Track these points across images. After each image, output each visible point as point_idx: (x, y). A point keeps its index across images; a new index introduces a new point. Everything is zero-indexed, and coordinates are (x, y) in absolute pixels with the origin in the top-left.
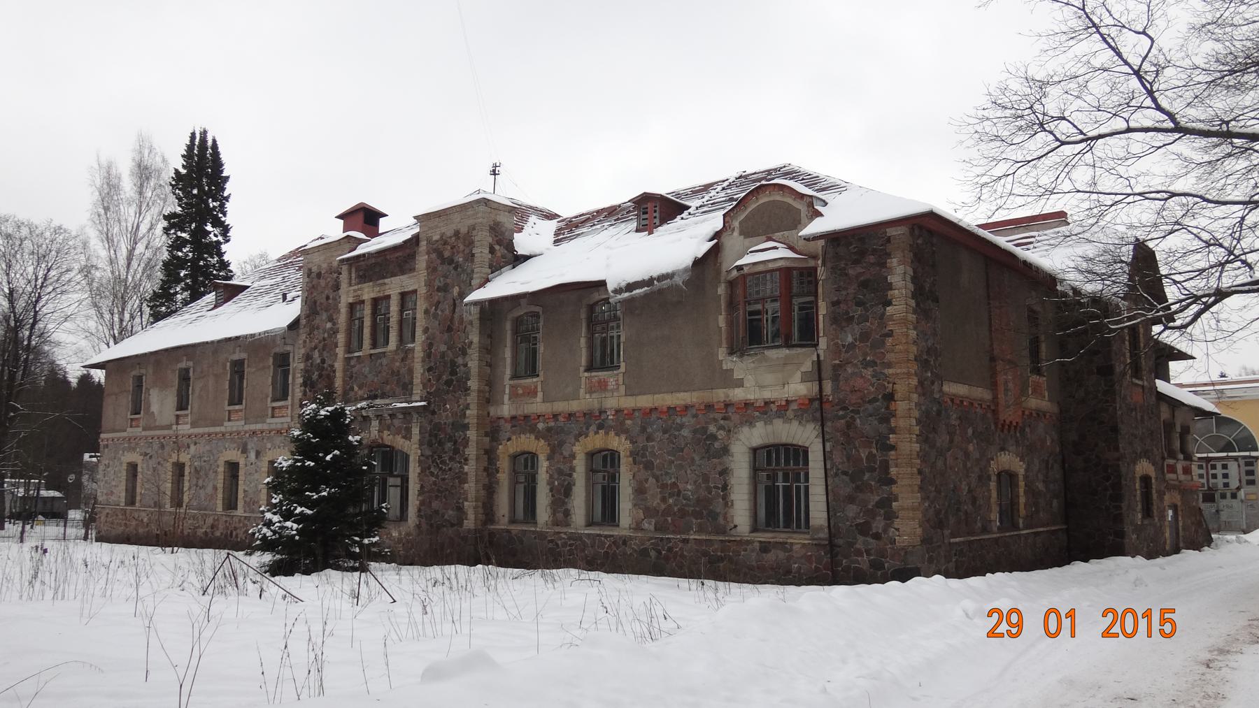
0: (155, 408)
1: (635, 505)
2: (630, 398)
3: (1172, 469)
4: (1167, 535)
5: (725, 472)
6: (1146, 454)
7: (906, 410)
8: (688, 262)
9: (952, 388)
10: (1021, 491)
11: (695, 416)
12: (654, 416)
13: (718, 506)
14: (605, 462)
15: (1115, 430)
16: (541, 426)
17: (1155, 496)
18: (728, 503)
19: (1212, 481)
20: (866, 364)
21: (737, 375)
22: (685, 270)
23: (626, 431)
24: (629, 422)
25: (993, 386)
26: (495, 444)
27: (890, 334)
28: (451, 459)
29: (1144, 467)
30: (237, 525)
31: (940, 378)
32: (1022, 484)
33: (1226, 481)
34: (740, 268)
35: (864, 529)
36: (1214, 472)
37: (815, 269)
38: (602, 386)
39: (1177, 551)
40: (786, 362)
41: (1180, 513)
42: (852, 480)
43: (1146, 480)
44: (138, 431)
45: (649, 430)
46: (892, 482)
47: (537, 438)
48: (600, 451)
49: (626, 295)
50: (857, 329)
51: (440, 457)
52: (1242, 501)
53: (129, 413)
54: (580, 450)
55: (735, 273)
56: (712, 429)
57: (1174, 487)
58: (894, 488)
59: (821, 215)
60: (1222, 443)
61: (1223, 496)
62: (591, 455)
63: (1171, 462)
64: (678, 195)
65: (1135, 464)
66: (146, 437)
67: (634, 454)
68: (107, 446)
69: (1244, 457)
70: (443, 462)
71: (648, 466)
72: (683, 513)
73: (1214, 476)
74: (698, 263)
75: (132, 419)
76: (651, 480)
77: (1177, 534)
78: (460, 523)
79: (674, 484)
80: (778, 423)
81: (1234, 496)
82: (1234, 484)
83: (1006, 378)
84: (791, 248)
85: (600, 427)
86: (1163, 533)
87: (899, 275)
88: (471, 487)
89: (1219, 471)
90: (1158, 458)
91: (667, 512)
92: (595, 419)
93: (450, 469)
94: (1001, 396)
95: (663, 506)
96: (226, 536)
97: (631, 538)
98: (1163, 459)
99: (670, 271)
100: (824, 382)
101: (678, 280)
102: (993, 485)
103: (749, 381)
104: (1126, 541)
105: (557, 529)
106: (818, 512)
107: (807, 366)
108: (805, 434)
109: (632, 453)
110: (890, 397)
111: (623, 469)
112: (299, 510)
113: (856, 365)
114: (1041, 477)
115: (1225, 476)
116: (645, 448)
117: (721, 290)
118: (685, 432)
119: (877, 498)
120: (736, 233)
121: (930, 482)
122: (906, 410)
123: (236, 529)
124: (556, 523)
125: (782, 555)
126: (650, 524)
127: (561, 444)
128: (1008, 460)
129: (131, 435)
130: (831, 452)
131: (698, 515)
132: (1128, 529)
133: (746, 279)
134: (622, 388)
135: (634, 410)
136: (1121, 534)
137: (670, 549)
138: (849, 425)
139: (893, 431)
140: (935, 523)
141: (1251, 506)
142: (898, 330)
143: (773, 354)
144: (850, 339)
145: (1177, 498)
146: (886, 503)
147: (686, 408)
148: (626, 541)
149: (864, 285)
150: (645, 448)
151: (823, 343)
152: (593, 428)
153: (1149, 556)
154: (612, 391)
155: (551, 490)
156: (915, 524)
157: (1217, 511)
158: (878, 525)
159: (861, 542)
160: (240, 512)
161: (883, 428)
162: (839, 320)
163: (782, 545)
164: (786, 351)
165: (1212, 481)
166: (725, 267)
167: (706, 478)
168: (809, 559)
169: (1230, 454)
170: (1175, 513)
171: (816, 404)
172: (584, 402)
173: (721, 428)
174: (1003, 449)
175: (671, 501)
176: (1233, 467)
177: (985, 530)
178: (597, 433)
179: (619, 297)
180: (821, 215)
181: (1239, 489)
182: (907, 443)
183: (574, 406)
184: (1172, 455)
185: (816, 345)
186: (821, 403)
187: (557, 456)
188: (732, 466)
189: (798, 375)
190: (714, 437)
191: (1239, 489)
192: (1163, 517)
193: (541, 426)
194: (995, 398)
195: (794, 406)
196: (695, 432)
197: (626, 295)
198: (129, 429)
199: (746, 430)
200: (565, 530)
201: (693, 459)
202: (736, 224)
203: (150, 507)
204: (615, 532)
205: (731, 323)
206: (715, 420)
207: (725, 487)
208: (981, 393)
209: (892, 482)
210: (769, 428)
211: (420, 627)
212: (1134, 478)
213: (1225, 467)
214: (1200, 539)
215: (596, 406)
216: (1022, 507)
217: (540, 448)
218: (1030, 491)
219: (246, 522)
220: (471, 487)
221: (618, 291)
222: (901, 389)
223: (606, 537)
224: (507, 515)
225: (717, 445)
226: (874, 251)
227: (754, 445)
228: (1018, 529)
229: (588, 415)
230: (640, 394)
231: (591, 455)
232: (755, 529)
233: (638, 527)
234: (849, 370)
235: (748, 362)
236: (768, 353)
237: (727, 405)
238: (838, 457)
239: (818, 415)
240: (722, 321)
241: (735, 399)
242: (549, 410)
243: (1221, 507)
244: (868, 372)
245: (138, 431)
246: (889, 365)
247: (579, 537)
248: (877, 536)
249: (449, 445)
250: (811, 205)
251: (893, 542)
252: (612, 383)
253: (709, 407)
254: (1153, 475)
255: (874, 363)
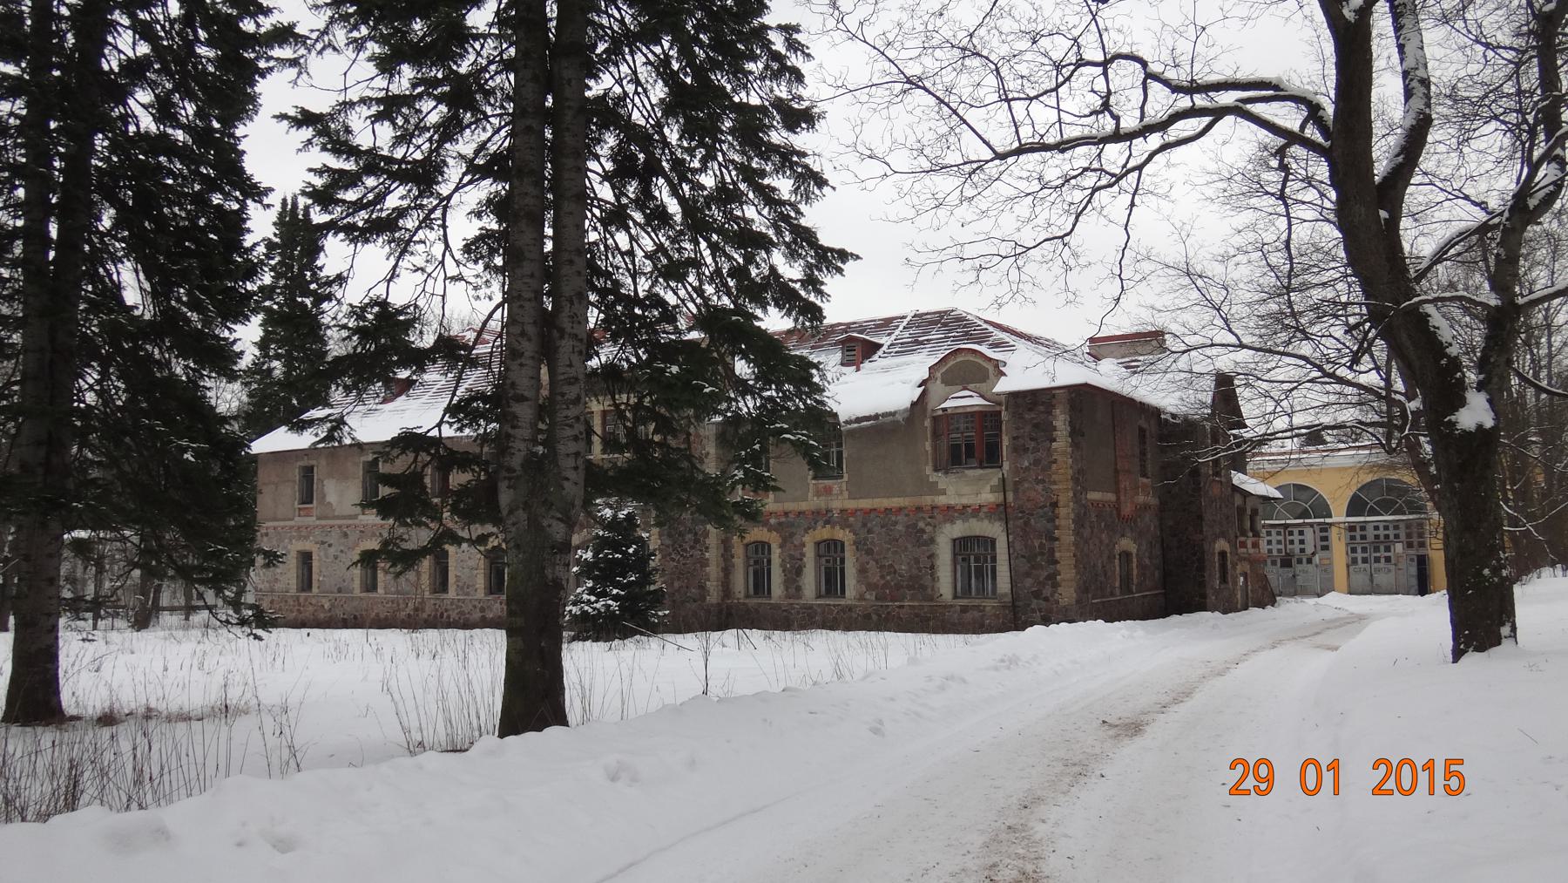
0: (332, 497)
1: (858, 582)
2: (852, 501)
3: (1243, 545)
4: (1239, 596)
5: (932, 556)
6: (1223, 535)
7: (1066, 513)
8: (908, 405)
9: (1094, 496)
10: (1134, 565)
11: (907, 515)
12: (872, 515)
13: (927, 581)
14: (831, 549)
15: (1200, 517)
16: (772, 521)
17: (1229, 566)
18: (934, 579)
19: (1289, 547)
20: (1038, 482)
21: (941, 486)
22: (905, 410)
23: (849, 526)
24: (851, 519)
25: (1117, 492)
26: (729, 535)
27: (1055, 461)
28: (692, 548)
29: (1222, 545)
30: (449, 607)
31: (1085, 490)
32: (1135, 560)
33: (1302, 546)
34: (944, 410)
35: (1037, 595)
36: (1291, 538)
37: (1000, 412)
38: (828, 491)
39: (1246, 608)
40: (980, 479)
41: (1249, 580)
42: (1029, 562)
43: (1223, 554)
44: (311, 520)
45: (869, 525)
46: (1057, 562)
47: (769, 531)
48: (825, 541)
49: (856, 425)
50: (1032, 457)
51: (681, 546)
52: (1317, 566)
53: (296, 503)
54: (809, 540)
55: (940, 413)
56: (921, 525)
57: (1245, 559)
58: (1058, 566)
59: (1004, 374)
60: (1299, 511)
61: (1299, 561)
62: (818, 544)
63: (1243, 539)
64: (861, 327)
65: (1215, 543)
66: (323, 527)
67: (857, 544)
68: (267, 535)
69: (1319, 524)
70: (685, 550)
71: (869, 552)
72: (898, 587)
73: (1279, 542)
74: (913, 404)
75: (300, 509)
76: (872, 563)
77: (1247, 595)
78: (703, 598)
79: (891, 566)
80: (973, 521)
81: (1309, 561)
82: (1309, 550)
83: (1125, 483)
84: (982, 396)
85: (827, 522)
86: (1236, 595)
87: (1061, 421)
88: (713, 570)
89: (1296, 538)
90: (1232, 536)
91: (886, 585)
92: (823, 516)
93: (692, 556)
94: (1122, 498)
95: (882, 582)
96: (435, 616)
97: (857, 606)
98: (1236, 537)
99: (893, 410)
100: (1007, 493)
101: (899, 418)
102: (1117, 562)
103: (951, 490)
104: (1208, 601)
105: (791, 601)
106: (1004, 583)
107: (995, 481)
108: (995, 530)
109: (855, 543)
110: (1055, 505)
111: (847, 554)
112: (615, 591)
113: (1030, 482)
114: (1147, 554)
115: (1302, 542)
116: (866, 539)
117: (928, 423)
118: (899, 527)
119: (1046, 574)
120: (939, 382)
121: (1081, 562)
122: (1066, 513)
123: (446, 610)
124: (788, 597)
125: (976, 614)
126: (871, 595)
127: (792, 535)
128: (1127, 544)
129: (300, 524)
130: (1013, 542)
131: (910, 587)
132: (1209, 592)
133: (950, 417)
134: (846, 494)
135: (856, 510)
136: (1204, 596)
137: (889, 613)
138: (1027, 523)
139: (1057, 528)
140: (1083, 589)
141: (1325, 571)
142: (1059, 458)
143: (970, 473)
144: (1026, 464)
145: (1247, 567)
146: (1052, 576)
147: (900, 509)
148: (850, 608)
149: (1036, 426)
150: (866, 539)
151: (1006, 466)
152: (820, 523)
153: (1225, 612)
154: (837, 495)
155: (784, 571)
156: (1072, 590)
157: (1294, 576)
158: (1047, 591)
159: (1035, 603)
160: (452, 593)
161: (1049, 526)
162: (1019, 450)
163: (977, 607)
164: (980, 471)
165: (1289, 547)
166: (930, 407)
167: (917, 561)
168: (997, 616)
169: (1307, 521)
170: (1246, 579)
171: (1002, 508)
172: (812, 502)
173: (929, 524)
174: (1123, 536)
175: (888, 578)
176: (1308, 532)
177: (1112, 594)
178: (824, 527)
179: (849, 426)
180: (1004, 374)
181: (1313, 554)
182: (1066, 535)
183: (804, 506)
184: (1244, 533)
185: (1001, 467)
186: (1005, 508)
187: (788, 545)
188: (938, 552)
189: (988, 488)
190: (923, 531)
191: (1313, 554)
192: (1235, 583)
193: (772, 521)
194: (1118, 498)
195: (985, 510)
196: (908, 527)
197: (856, 425)
198: (297, 519)
199: (948, 525)
200: (797, 602)
201: (906, 548)
202: (938, 375)
203: (332, 593)
204: (842, 602)
205: (935, 448)
206: (924, 519)
207: (932, 567)
208: (1111, 497)
209: (1057, 562)
210: (967, 524)
211: (199, 767)
212: (1213, 554)
213: (1301, 533)
214: (1265, 597)
215: (823, 506)
216: (1135, 577)
217: (774, 539)
218: (1139, 565)
219: (460, 604)
220: (713, 570)
221: (847, 422)
222: (1063, 499)
223: (834, 606)
224: (743, 592)
225: (925, 537)
226: (1043, 403)
227: (955, 537)
228: (1133, 593)
229: (817, 513)
230: (861, 498)
231: (818, 544)
232: (955, 597)
233: (861, 598)
234: (1026, 485)
235: (952, 478)
236: (966, 472)
237: (933, 508)
238: (1018, 546)
239: (1003, 516)
240: (928, 446)
241: (939, 504)
242: (781, 509)
243: (1298, 572)
244: (1040, 487)
245: (311, 520)
246: (1055, 483)
247: (811, 607)
248: (1046, 599)
249: (689, 537)
250: (997, 366)
251: (1057, 602)
252: (836, 489)
253: (919, 509)
254: (1228, 550)
255: (1043, 481)
